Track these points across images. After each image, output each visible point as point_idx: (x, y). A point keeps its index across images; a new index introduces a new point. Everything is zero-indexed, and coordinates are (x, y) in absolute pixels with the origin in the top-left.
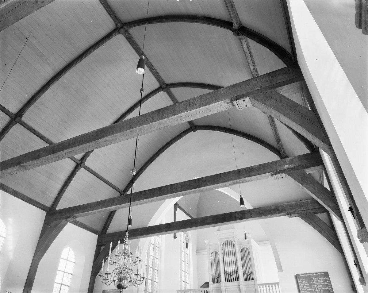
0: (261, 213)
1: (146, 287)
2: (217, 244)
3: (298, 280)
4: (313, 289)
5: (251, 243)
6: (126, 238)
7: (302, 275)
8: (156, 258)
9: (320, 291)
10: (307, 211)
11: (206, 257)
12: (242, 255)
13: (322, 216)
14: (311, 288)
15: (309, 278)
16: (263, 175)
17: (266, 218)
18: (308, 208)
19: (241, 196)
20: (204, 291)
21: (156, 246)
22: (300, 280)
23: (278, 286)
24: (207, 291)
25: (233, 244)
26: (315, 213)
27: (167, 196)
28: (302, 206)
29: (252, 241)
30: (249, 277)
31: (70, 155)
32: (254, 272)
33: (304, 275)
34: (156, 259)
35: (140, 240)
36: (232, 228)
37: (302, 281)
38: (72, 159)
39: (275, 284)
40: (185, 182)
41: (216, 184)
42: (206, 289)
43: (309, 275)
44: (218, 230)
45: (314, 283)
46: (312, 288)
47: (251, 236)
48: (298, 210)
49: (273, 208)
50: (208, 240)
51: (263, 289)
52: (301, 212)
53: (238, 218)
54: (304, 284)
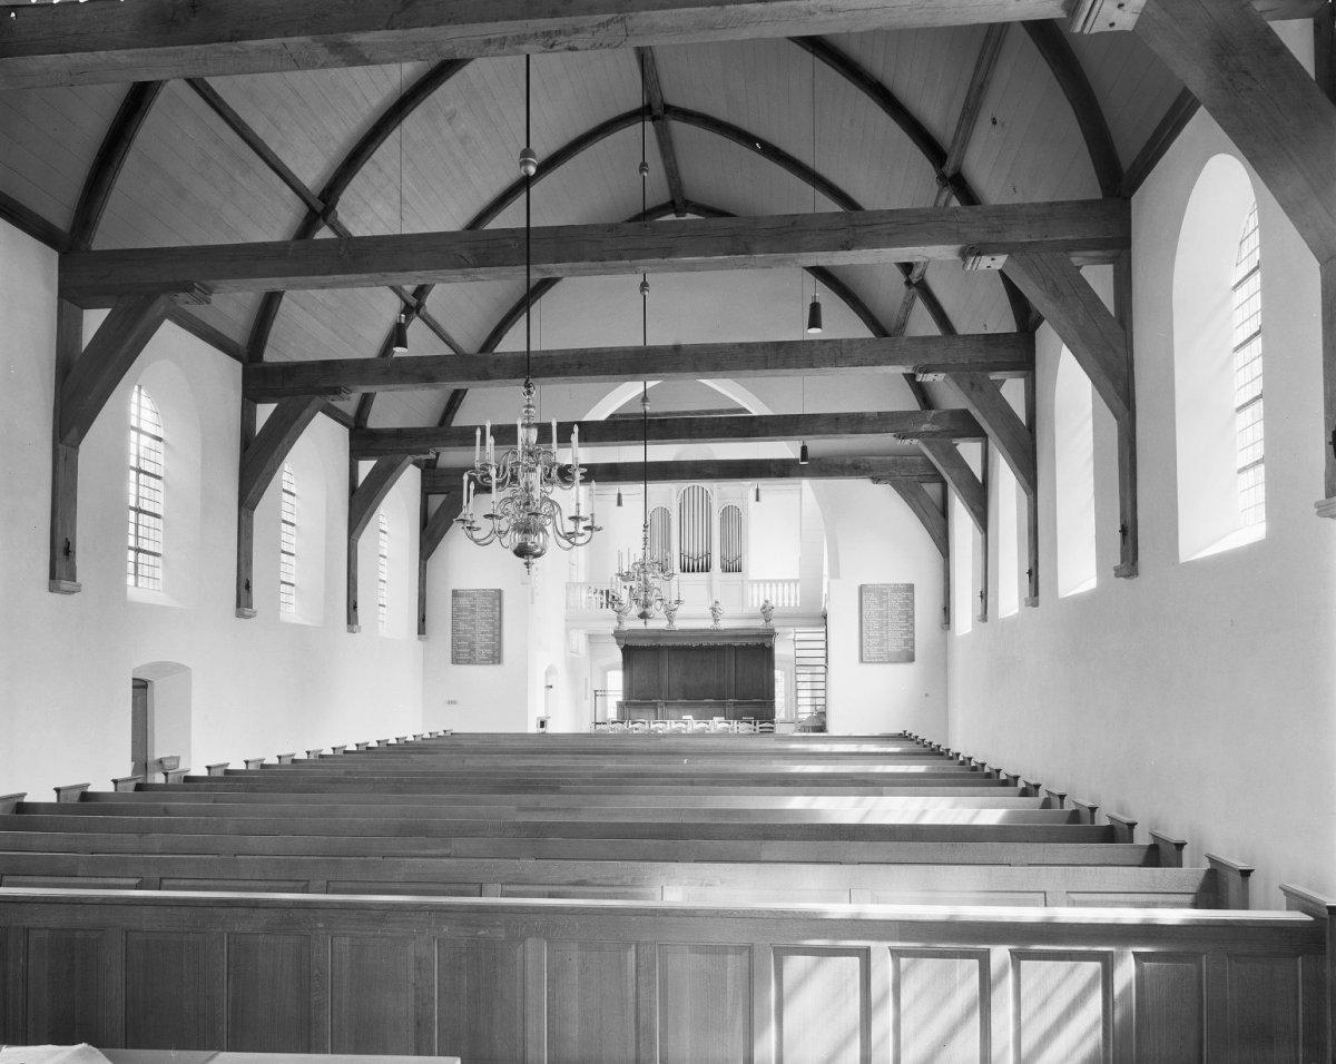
13: (932, 489)
15: (880, 591)
28: (903, 468)
30: (733, 566)
31: (395, 282)
38: (397, 290)
49: (849, 462)
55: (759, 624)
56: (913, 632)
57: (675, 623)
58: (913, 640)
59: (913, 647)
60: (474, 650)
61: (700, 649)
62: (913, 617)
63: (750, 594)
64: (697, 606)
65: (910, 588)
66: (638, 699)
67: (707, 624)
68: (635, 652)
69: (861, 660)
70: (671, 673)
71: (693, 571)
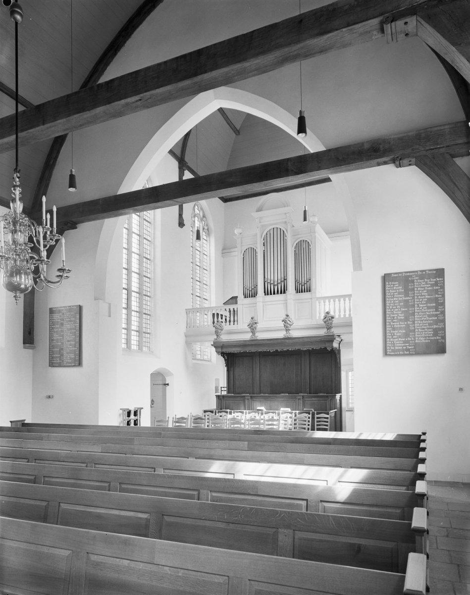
0: (340, 158)
1: (129, 304)
2: (256, 235)
3: (387, 283)
4: (409, 298)
5: (315, 232)
6: (15, 186)
7: (396, 275)
8: (146, 258)
9: (421, 300)
10: (436, 151)
11: (236, 260)
12: (296, 255)
14: (407, 295)
15: (406, 280)
16: (360, 25)
17: (350, 170)
18: (441, 144)
19: (301, 112)
20: (230, 309)
21: (145, 238)
22: (390, 283)
23: (350, 300)
24: (234, 309)
25: (283, 234)
26: (453, 156)
27: (127, 104)
29: (318, 228)
30: (303, 288)
32: (313, 280)
33: (400, 275)
34: (144, 259)
35: (105, 223)
36: (285, 207)
37: (392, 286)
39: (344, 296)
40: (165, 62)
41: (239, 62)
42: (232, 307)
43: (408, 274)
44: (260, 210)
45: (414, 289)
46: (408, 296)
47: (317, 220)
48: (418, 149)
49: (366, 146)
50: (239, 228)
51: (325, 305)
52: (424, 153)
53: (292, 170)
54: (395, 290)
55: (322, 332)
56: (444, 321)
57: (257, 334)
58: (444, 329)
59: (444, 337)
60: (62, 355)
61: (277, 354)
62: (443, 304)
63: (318, 310)
64: (273, 320)
65: (440, 273)
66: (235, 395)
67: (281, 335)
68: (234, 357)
69: (386, 354)
70: (265, 373)
71: (274, 294)
